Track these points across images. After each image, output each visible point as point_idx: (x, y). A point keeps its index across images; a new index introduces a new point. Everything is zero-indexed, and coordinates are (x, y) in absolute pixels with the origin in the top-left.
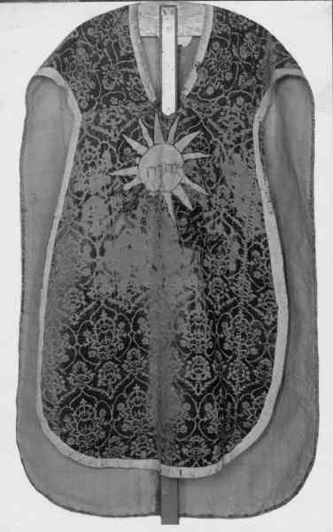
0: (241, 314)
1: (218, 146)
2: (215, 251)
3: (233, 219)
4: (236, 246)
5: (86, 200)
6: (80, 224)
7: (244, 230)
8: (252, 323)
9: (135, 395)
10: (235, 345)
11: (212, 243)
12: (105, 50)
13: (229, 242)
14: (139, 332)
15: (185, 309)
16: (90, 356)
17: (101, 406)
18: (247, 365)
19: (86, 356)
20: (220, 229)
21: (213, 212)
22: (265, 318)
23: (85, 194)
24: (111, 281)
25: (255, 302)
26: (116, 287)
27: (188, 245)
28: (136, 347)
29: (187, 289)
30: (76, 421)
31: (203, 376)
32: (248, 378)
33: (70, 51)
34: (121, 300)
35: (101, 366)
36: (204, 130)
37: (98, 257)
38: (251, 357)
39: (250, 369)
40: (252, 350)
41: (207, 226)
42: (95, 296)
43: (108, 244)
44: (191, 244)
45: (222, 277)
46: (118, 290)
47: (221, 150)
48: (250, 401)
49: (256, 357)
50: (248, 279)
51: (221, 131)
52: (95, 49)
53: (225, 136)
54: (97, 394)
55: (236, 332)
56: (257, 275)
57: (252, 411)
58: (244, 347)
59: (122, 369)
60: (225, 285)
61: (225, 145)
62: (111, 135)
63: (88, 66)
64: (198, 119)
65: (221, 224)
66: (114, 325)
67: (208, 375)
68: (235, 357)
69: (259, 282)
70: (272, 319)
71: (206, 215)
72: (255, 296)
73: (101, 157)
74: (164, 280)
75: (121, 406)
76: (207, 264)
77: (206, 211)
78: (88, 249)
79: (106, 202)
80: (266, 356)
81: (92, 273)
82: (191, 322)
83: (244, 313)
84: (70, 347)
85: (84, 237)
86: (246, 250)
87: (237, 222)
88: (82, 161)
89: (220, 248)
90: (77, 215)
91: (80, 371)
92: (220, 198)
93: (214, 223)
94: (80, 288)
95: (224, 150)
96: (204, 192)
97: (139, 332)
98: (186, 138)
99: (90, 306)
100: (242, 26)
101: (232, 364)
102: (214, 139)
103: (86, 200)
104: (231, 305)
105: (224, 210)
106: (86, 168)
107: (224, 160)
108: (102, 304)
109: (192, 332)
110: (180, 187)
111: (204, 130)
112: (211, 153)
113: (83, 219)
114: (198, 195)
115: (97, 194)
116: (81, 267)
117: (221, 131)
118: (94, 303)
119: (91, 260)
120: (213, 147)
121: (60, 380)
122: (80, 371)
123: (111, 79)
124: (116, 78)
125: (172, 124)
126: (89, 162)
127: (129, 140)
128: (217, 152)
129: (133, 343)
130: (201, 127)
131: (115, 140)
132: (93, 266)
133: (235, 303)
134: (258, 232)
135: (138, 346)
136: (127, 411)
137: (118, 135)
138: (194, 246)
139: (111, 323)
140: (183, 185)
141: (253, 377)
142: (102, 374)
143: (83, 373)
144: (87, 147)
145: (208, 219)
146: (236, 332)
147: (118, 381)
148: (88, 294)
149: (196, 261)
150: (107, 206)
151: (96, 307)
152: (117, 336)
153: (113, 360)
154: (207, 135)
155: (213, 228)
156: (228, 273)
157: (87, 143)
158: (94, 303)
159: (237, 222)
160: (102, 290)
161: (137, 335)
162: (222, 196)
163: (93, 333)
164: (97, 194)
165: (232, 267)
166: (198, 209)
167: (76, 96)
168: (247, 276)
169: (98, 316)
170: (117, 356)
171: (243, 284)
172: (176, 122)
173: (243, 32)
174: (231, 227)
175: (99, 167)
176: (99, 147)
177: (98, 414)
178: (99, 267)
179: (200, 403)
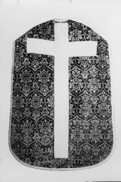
31: (76, 121)
35: (79, 76)
121: (93, 124)
135: (83, 30)
142: (42, 87)
143: (19, 87)
161: (75, 108)
170: (73, 29)
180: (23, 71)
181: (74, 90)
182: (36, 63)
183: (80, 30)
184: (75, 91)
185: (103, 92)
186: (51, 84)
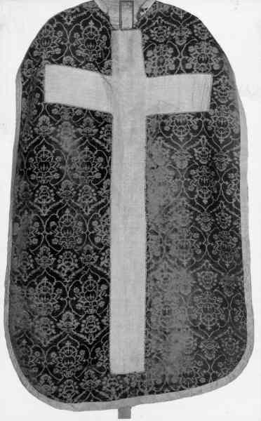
9: (211, 323)
16: (198, 234)
17: (82, 348)
33: (173, 16)
48: (220, 321)
66: (53, 289)
100: (194, 346)
104: (219, 333)
147: (98, 331)
173: (198, 348)
179: (47, 352)
180: (37, 151)
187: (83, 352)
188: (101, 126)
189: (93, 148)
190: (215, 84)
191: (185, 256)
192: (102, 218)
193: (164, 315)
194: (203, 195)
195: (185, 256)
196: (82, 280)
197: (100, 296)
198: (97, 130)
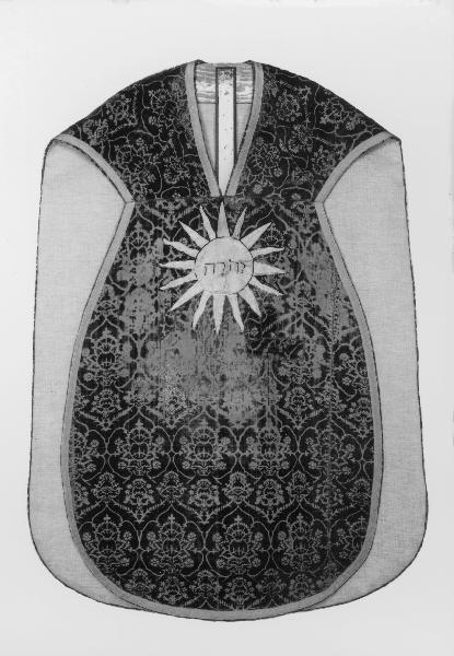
0: (329, 429)
1: (293, 236)
2: (294, 356)
3: (316, 319)
4: (321, 349)
5: (130, 291)
6: (121, 318)
7: (329, 330)
8: (343, 438)
9: (169, 527)
10: (323, 463)
11: (291, 347)
12: (170, 141)
13: (312, 345)
14: (180, 453)
15: (255, 427)
18: (339, 486)
19: (115, 467)
20: (301, 332)
21: (292, 313)
22: (359, 431)
23: (130, 283)
24: (152, 387)
25: (345, 413)
26: (157, 394)
27: (258, 353)
28: (174, 470)
29: (255, 403)
30: (97, 539)
31: (275, 501)
32: (341, 501)
34: (161, 411)
36: (277, 221)
37: (139, 357)
38: (343, 477)
39: (343, 492)
40: (344, 470)
41: (285, 331)
42: (132, 401)
43: (151, 345)
44: (261, 353)
45: (304, 387)
46: (159, 399)
47: (297, 241)
49: (349, 477)
50: (336, 387)
51: (296, 219)
52: (157, 139)
53: (301, 224)
54: (123, 513)
55: (325, 449)
56: (346, 381)
57: (349, 540)
58: (334, 467)
59: (156, 492)
60: (308, 395)
61: (302, 234)
62: (167, 221)
63: (147, 158)
64: (268, 208)
65: (302, 326)
67: (281, 499)
68: (324, 478)
69: (349, 389)
70: (367, 432)
71: (281, 319)
72: (345, 406)
73: (152, 245)
74: (223, 394)
75: (151, 536)
76: (282, 372)
77: (281, 314)
78: (128, 347)
79: (152, 297)
80: (362, 475)
81: (131, 375)
82: (262, 440)
83: (333, 427)
84: (98, 455)
85: (124, 334)
86: (332, 353)
87: (321, 322)
88: (131, 246)
89: (300, 353)
90: (117, 307)
91: (107, 483)
92: (299, 296)
93: (293, 326)
94: (116, 391)
95: (300, 239)
96: (277, 293)
97: (180, 453)
98: (254, 232)
99: (125, 413)
101: (320, 486)
102: (288, 228)
103: (130, 291)
105: (306, 310)
106: (134, 254)
107: (301, 252)
108: (139, 411)
109: (263, 452)
110: (247, 288)
111: (277, 221)
112: (286, 245)
113: (125, 313)
114: (270, 298)
115: (144, 286)
116: (120, 367)
117: (296, 219)
118: (129, 409)
119: (130, 360)
120: (288, 238)
122: (107, 483)
123: (174, 173)
124: (181, 172)
125: (239, 215)
126: (138, 248)
127: (187, 229)
128: (293, 244)
129: (172, 464)
130: (272, 218)
131: (171, 227)
132: (132, 367)
133: (322, 415)
134: (346, 332)
136: (159, 544)
137: (175, 221)
138: (264, 354)
139: (147, 435)
140: (251, 287)
141: (347, 501)
142: (131, 490)
144: (138, 231)
145: (286, 322)
146: (325, 449)
148: (125, 398)
149: (266, 372)
150: (153, 301)
151: (131, 414)
152: (154, 453)
153: (145, 477)
154: (280, 226)
155: (292, 331)
156: (312, 382)
157: (138, 225)
158: (129, 409)
159: (321, 322)
160: (141, 396)
161: (177, 456)
162: (302, 294)
163: (125, 442)
164: (144, 286)
165: (317, 374)
166: (271, 314)
167: (131, 191)
168: (334, 384)
169: (132, 425)
171: (329, 394)
172: (243, 213)
174: (314, 329)
175: (149, 257)
176: (152, 232)
177: (122, 535)
178: (140, 370)
180: (161, 522)
181: (145, 232)
182: (109, 401)
183: (93, 381)
184: (243, 521)
185: (270, 517)
186: (228, 477)
187: (95, 443)
188: (94, 394)
189: (308, 515)
190: (102, 152)
191: (172, 530)
192: (96, 344)
193: (176, 542)
194: (175, 527)
195: (172, 530)
196: (333, 129)
197: (154, 453)
198: (251, 490)
